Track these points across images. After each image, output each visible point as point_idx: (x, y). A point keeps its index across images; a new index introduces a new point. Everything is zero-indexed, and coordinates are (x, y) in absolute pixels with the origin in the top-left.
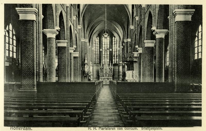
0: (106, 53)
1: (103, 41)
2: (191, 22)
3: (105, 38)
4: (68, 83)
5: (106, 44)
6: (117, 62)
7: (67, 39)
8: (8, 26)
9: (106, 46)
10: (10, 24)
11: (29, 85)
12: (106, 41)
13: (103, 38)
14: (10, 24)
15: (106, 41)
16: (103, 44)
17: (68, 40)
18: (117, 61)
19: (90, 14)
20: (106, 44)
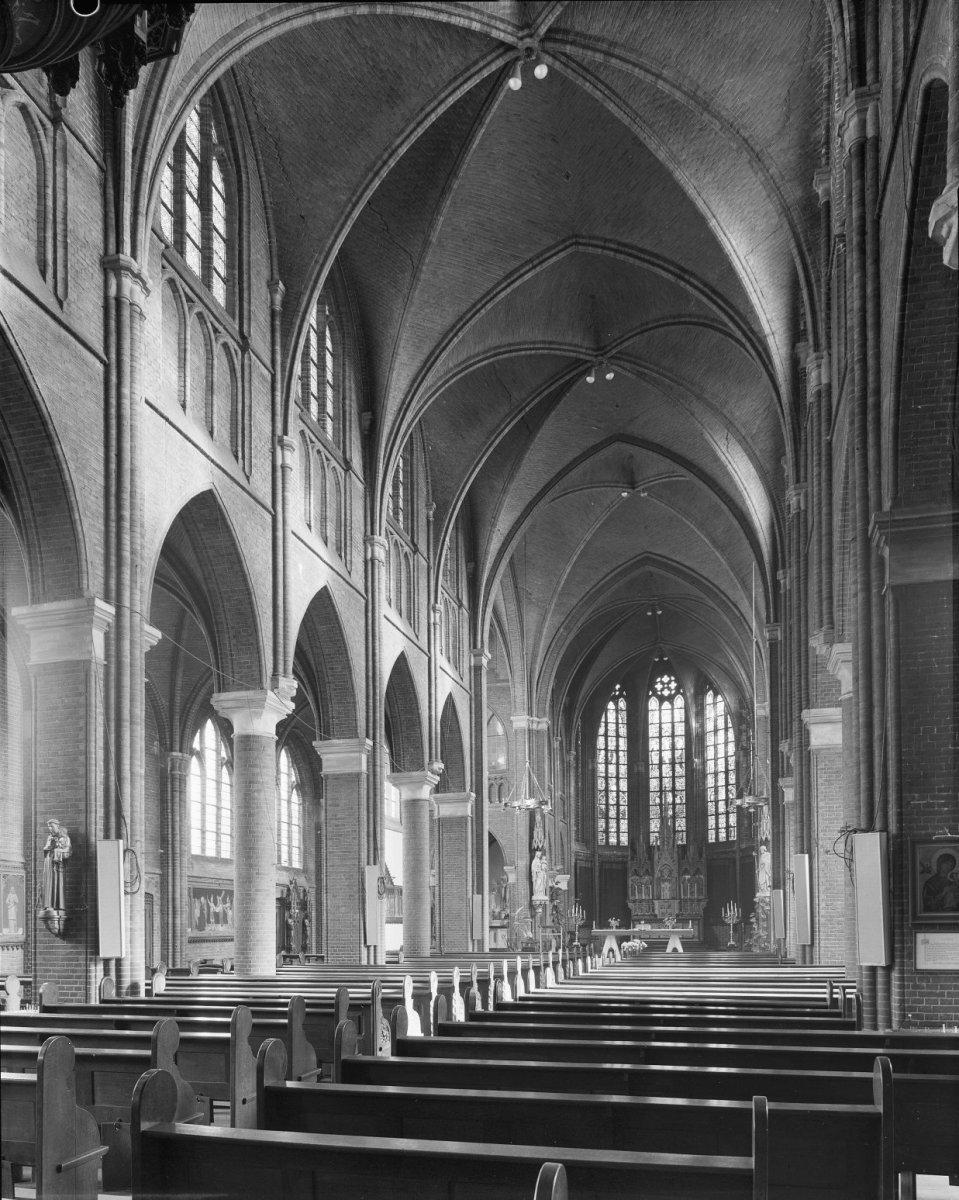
0: (612, 769)
1: (653, 718)
2: (286, 1080)
3: (662, 699)
4: (706, 910)
5: (667, 729)
6: (728, 833)
7: (371, 732)
8: (198, 734)
9: (667, 743)
10: (209, 722)
11: (71, 977)
12: (666, 717)
13: (653, 703)
14: (209, 722)
15: (666, 717)
16: (653, 731)
17: (374, 738)
18: (728, 827)
19: (763, 848)
20: (667, 729)
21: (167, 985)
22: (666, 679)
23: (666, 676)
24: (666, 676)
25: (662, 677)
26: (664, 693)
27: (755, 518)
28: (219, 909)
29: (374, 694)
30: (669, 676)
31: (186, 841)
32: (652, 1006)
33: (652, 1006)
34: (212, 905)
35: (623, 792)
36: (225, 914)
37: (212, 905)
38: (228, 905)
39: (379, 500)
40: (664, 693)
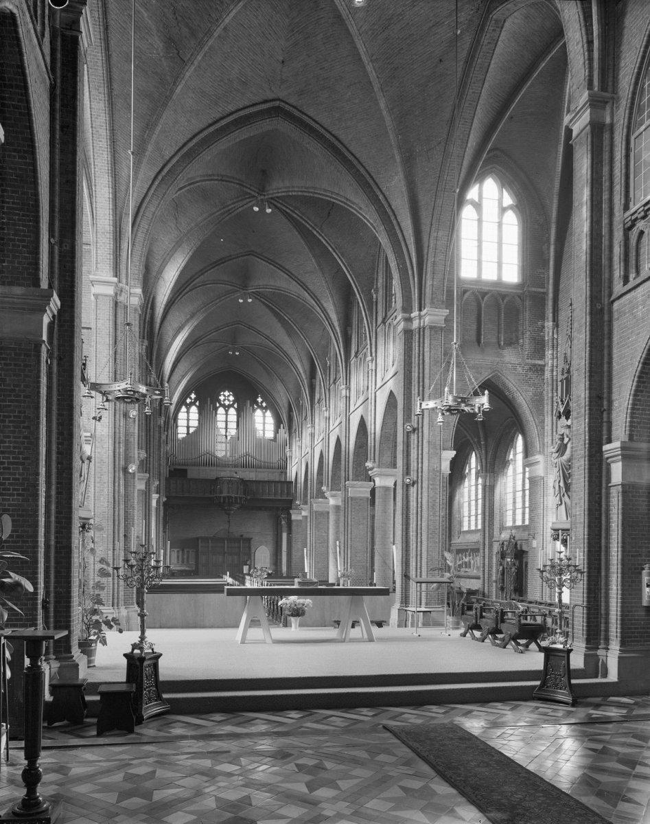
21: (412, 626)
22: (227, 393)
23: (220, 398)
24: (220, 398)
25: (233, 396)
26: (193, 398)
27: (185, 336)
28: (467, 560)
29: (344, 559)
30: (220, 395)
31: (461, 523)
32: (285, 535)
33: (285, 535)
34: (464, 558)
35: (580, 523)
36: (470, 563)
37: (464, 558)
38: (471, 557)
39: (618, 188)
40: (193, 398)
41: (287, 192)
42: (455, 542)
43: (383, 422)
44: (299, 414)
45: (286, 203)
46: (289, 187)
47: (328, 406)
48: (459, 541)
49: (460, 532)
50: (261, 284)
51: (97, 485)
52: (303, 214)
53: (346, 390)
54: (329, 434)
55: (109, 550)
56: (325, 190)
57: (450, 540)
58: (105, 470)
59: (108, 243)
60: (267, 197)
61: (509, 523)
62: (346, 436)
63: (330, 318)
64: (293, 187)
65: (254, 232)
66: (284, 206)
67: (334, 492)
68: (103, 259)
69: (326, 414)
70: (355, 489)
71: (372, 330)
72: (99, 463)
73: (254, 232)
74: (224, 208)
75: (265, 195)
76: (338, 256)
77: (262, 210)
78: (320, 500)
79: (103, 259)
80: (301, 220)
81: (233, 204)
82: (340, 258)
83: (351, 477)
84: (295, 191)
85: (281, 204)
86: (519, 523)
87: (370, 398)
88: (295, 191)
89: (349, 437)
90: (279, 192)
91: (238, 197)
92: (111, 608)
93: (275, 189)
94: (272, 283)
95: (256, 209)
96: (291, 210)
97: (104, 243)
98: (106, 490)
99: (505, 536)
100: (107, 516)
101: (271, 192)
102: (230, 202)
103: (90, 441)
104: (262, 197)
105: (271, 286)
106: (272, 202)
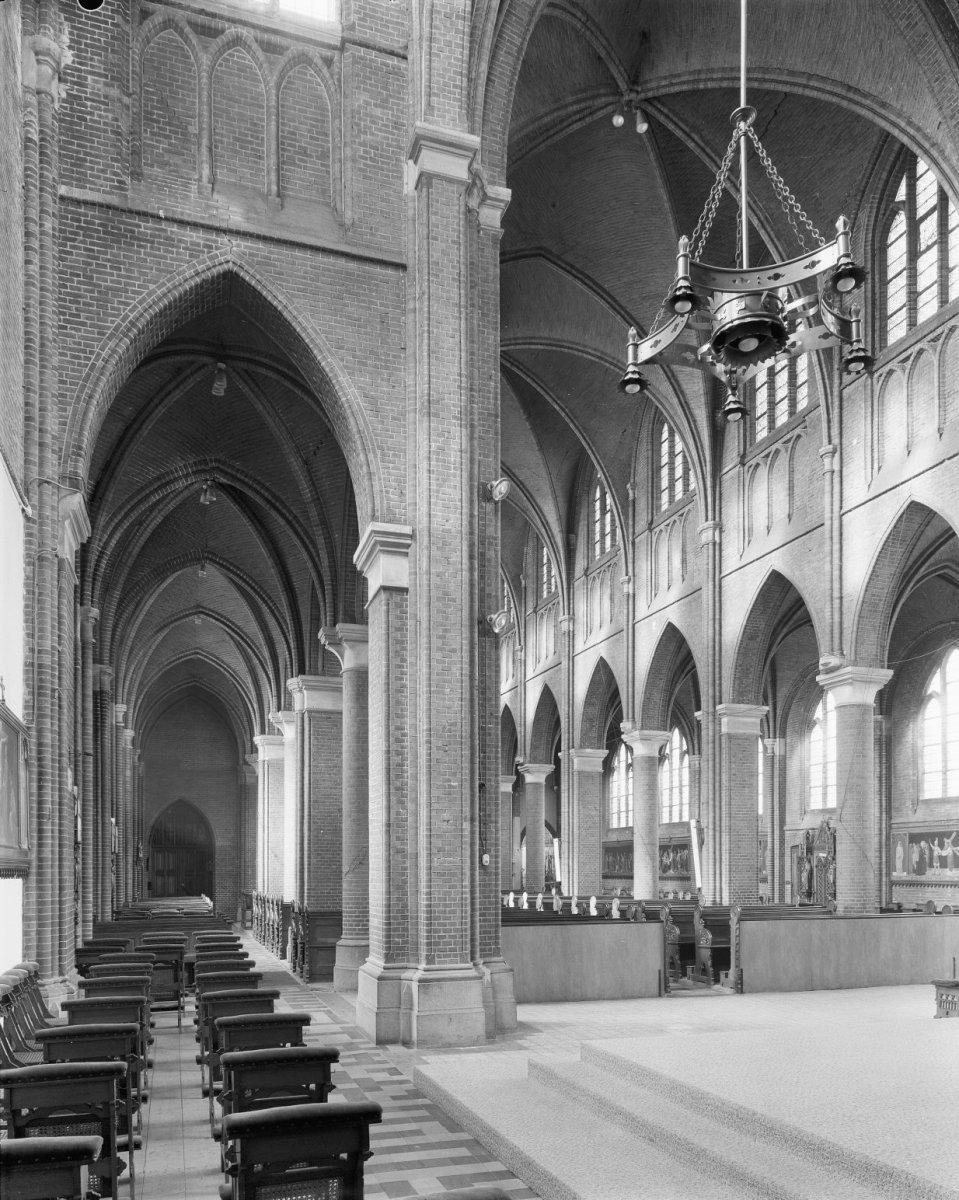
41: (694, 81)
42: (901, 820)
43: (873, 571)
44: (520, 604)
45: (676, 115)
46: (699, 72)
47: (630, 574)
48: (913, 818)
49: (916, 802)
50: (519, 335)
51: (436, 655)
52: (707, 143)
53: (715, 530)
54: (634, 625)
55: (463, 819)
56: (792, 73)
57: (890, 817)
58: (454, 618)
59: (457, 45)
60: (642, 96)
61: (666, 820)
62: (714, 619)
63: (682, 392)
64: (712, 70)
65: (554, 206)
66: (671, 120)
67: (646, 732)
68: (445, 84)
69: (628, 588)
70: (737, 719)
71: (832, 392)
72: (438, 599)
73: (554, 206)
74: (558, 109)
75: (637, 92)
76: (769, 236)
77: (630, 122)
78: (588, 750)
79: (445, 84)
80: (808, 92)
81: (575, 103)
82: (772, 240)
83: (725, 697)
84: (713, 80)
85: (667, 116)
86: (676, 820)
87: (828, 523)
88: (713, 80)
89: (720, 619)
90: (672, 84)
91: (584, 91)
92: (470, 965)
93: (665, 78)
94: (545, 333)
95: (619, 121)
96: (685, 132)
97: (449, 44)
98: (456, 670)
99: (810, 822)
100: (458, 734)
101: (654, 84)
102: (570, 99)
103: (408, 546)
104: (633, 96)
105: (540, 338)
106: (650, 106)
